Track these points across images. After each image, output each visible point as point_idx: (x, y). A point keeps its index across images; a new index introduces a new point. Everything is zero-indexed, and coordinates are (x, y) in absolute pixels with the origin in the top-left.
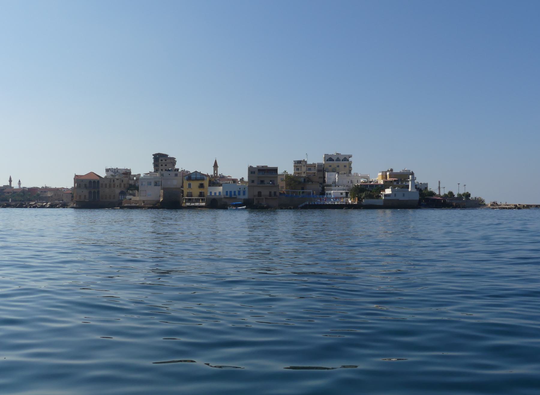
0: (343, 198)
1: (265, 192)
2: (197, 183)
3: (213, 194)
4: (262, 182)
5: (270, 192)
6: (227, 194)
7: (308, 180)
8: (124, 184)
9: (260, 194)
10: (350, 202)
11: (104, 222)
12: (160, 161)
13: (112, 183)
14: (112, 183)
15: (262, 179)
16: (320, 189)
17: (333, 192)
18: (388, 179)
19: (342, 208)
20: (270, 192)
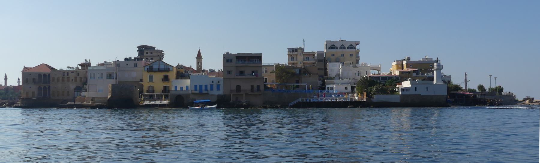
0: (348, 93)
1: (245, 86)
2: (161, 75)
3: (179, 89)
4: (242, 73)
5: (252, 87)
6: (196, 89)
7: (304, 71)
8: (81, 78)
9: (238, 88)
10: (356, 98)
11: (62, 124)
12: (145, 54)
13: (66, 77)
14: (66, 77)
15: (242, 69)
16: (320, 82)
17: (335, 87)
18: (405, 69)
19: (346, 107)
20: (252, 87)
